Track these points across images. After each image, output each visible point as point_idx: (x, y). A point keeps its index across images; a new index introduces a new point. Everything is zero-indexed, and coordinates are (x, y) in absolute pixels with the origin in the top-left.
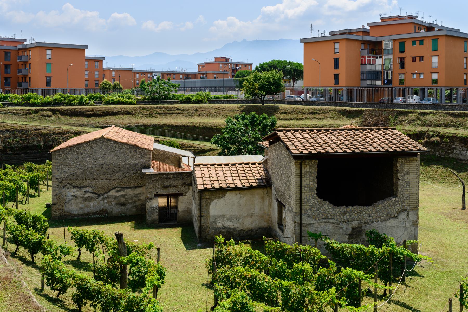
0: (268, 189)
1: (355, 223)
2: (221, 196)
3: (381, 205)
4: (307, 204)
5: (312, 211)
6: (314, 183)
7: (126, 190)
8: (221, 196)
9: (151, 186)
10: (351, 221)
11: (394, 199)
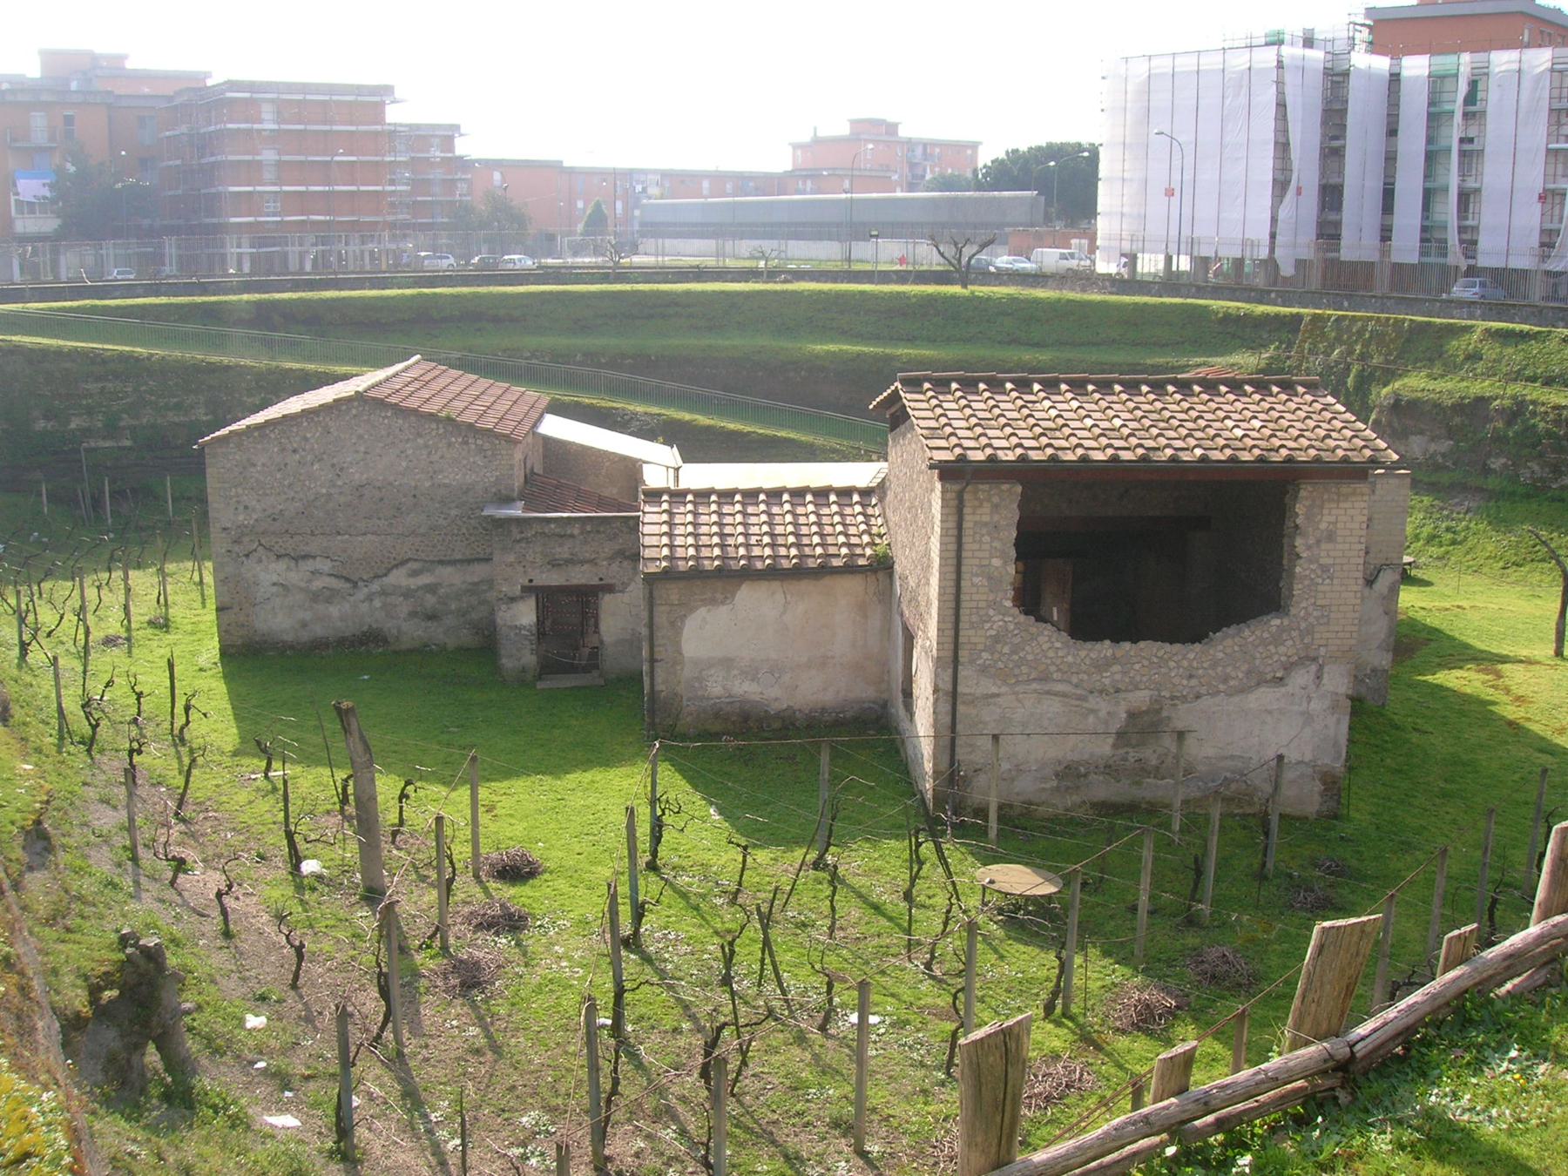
0: (881, 575)
1: (1141, 698)
2: (719, 596)
3: (1228, 645)
4: (980, 632)
5: (996, 656)
8: (719, 596)
10: (1126, 691)
11: (1277, 622)
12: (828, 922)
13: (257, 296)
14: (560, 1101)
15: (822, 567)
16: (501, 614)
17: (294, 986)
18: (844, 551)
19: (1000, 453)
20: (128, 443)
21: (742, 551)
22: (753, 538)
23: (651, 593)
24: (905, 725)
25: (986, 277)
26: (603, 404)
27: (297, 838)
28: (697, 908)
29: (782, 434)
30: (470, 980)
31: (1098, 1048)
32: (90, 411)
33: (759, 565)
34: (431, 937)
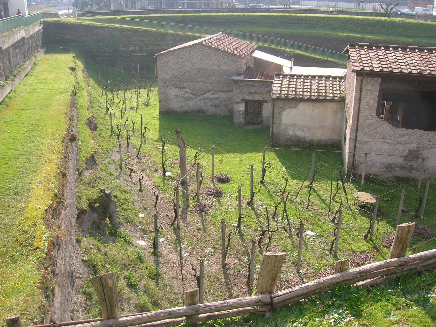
0: (342, 103)
1: (413, 147)
2: (294, 106)
4: (365, 123)
5: (370, 130)
6: (374, 102)
7: (220, 93)
9: (238, 91)
12: (307, 203)
13: (183, 14)
14: (218, 246)
15: (324, 99)
16: (235, 107)
17: (155, 206)
18: (331, 95)
19: (375, 69)
20: (145, 54)
21: (301, 93)
22: (305, 89)
23: (273, 104)
24: (344, 148)
25: (396, 15)
26: (278, 48)
27: (165, 166)
28: (271, 196)
29: (329, 59)
30: (202, 210)
31: (378, 251)
32: (135, 45)
33: (305, 97)
34: (195, 196)
